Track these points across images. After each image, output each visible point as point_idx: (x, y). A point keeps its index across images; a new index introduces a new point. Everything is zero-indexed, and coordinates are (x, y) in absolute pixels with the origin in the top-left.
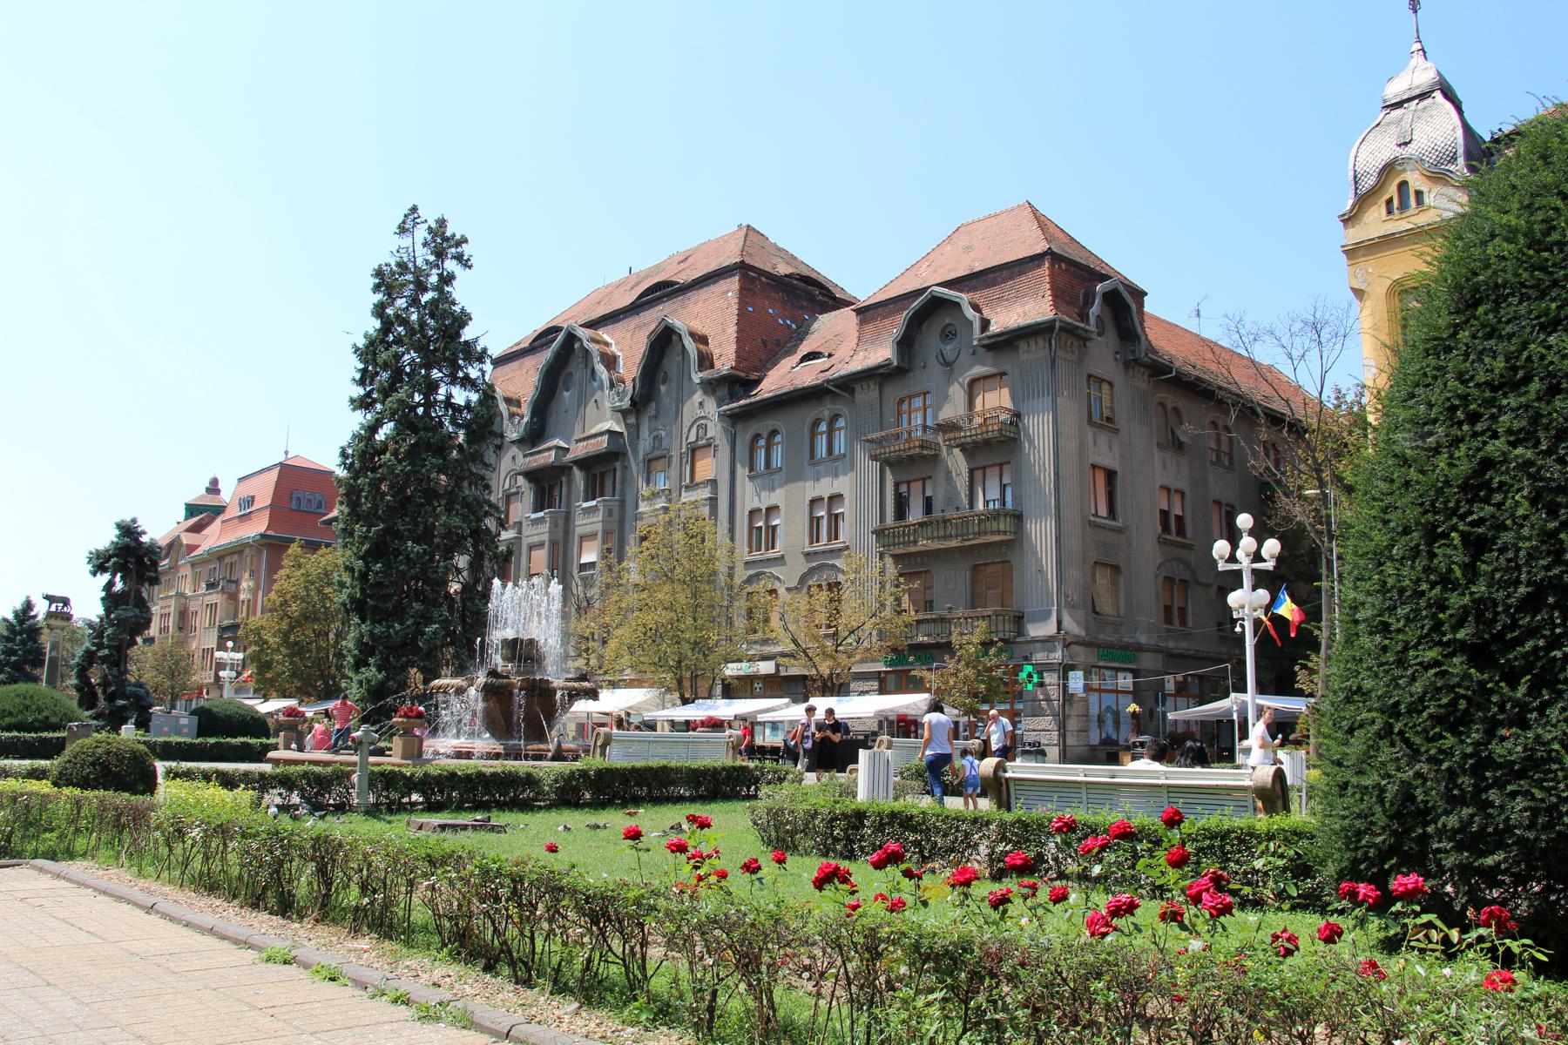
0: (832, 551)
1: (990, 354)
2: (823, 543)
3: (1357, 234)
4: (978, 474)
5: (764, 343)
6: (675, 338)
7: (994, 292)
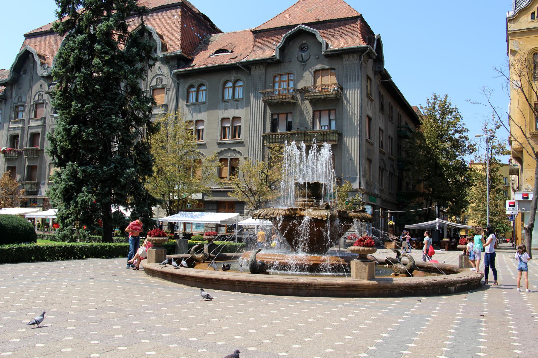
0: (234, 143)
1: (327, 60)
2: (228, 140)
3: (513, 27)
4: (317, 114)
5: (190, 43)
6: (30, 56)
7: (330, 31)
